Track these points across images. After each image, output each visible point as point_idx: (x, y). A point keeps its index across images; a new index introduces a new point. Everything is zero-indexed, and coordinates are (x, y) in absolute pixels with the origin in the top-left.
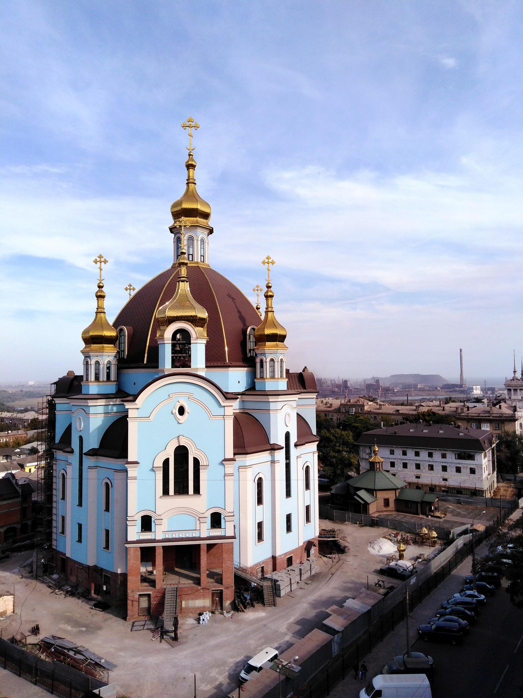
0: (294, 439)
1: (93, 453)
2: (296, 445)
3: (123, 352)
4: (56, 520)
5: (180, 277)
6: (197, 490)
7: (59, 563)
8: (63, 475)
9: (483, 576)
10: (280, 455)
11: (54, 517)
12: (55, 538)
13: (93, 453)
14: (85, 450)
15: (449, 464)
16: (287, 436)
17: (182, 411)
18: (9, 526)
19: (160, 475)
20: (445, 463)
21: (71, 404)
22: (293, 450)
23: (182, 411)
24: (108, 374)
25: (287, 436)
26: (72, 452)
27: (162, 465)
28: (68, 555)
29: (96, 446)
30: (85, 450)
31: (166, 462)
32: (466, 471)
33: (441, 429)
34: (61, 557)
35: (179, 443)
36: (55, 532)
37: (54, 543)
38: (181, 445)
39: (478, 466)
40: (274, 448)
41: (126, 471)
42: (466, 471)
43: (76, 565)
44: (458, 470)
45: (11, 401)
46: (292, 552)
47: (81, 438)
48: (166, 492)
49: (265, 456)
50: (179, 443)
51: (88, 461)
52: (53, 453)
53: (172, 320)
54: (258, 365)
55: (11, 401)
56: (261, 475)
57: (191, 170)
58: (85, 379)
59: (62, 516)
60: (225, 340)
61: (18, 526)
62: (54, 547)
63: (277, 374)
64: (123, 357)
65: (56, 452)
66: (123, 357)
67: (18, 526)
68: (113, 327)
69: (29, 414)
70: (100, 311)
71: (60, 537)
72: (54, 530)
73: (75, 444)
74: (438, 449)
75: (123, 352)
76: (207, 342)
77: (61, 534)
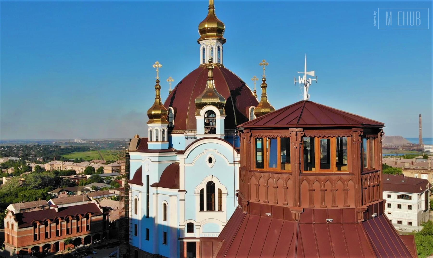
1: (156, 185)
3: (171, 124)
4: (131, 227)
5: (209, 78)
6: (220, 210)
7: (134, 253)
8: (136, 199)
9: (207, 74)
11: (130, 225)
12: (131, 238)
13: (156, 185)
15: (393, 202)
18: (96, 233)
19: (198, 198)
20: (390, 201)
21: (141, 155)
24: (157, 137)
26: (142, 184)
27: (199, 193)
28: (140, 248)
29: (157, 181)
31: (202, 191)
32: (404, 207)
33: (389, 177)
34: (135, 250)
35: (212, 180)
36: (131, 234)
37: (130, 241)
38: (212, 181)
39: (414, 204)
41: (176, 196)
42: (404, 207)
43: (146, 254)
44: (399, 206)
47: (148, 177)
48: (202, 209)
50: (212, 180)
51: (152, 190)
52: (129, 185)
53: (205, 104)
58: (149, 140)
59: (135, 225)
60: (235, 116)
61: (101, 233)
62: (130, 244)
64: (171, 126)
65: (131, 185)
66: (171, 126)
67: (101, 233)
69: (84, 163)
70: (158, 97)
71: (134, 237)
72: (130, 233)
73: (144, 180)
74: (385, 192)
75: (171, 124)
76: (226, 118)
77: (135, 236)
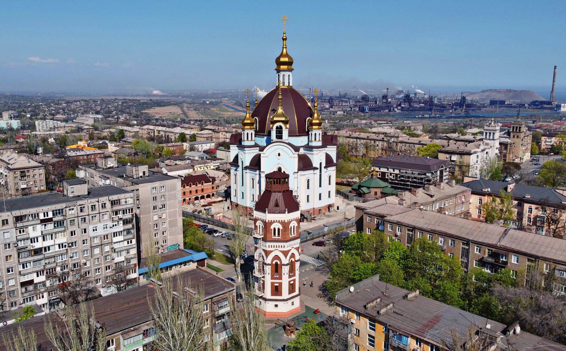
0: (324, 165)
1: (246, 168)
2: (325, 167)
10: (318, 172)
13: (246, 168)
14: (244, 166)
16: (321, 164)
17: (279, 155)
22: (323, 170)
23: (279, 155)
25: (321, 164)
30: (244, 166)
40: (316, 169)
45: (394, 119)
46: (322, 207)
49: (312, 171)
54: (310, 135)
55: (394, 119)
56: (280, 166)
57: (285, 41)
63: (317, 139)
68: (186, 250)
